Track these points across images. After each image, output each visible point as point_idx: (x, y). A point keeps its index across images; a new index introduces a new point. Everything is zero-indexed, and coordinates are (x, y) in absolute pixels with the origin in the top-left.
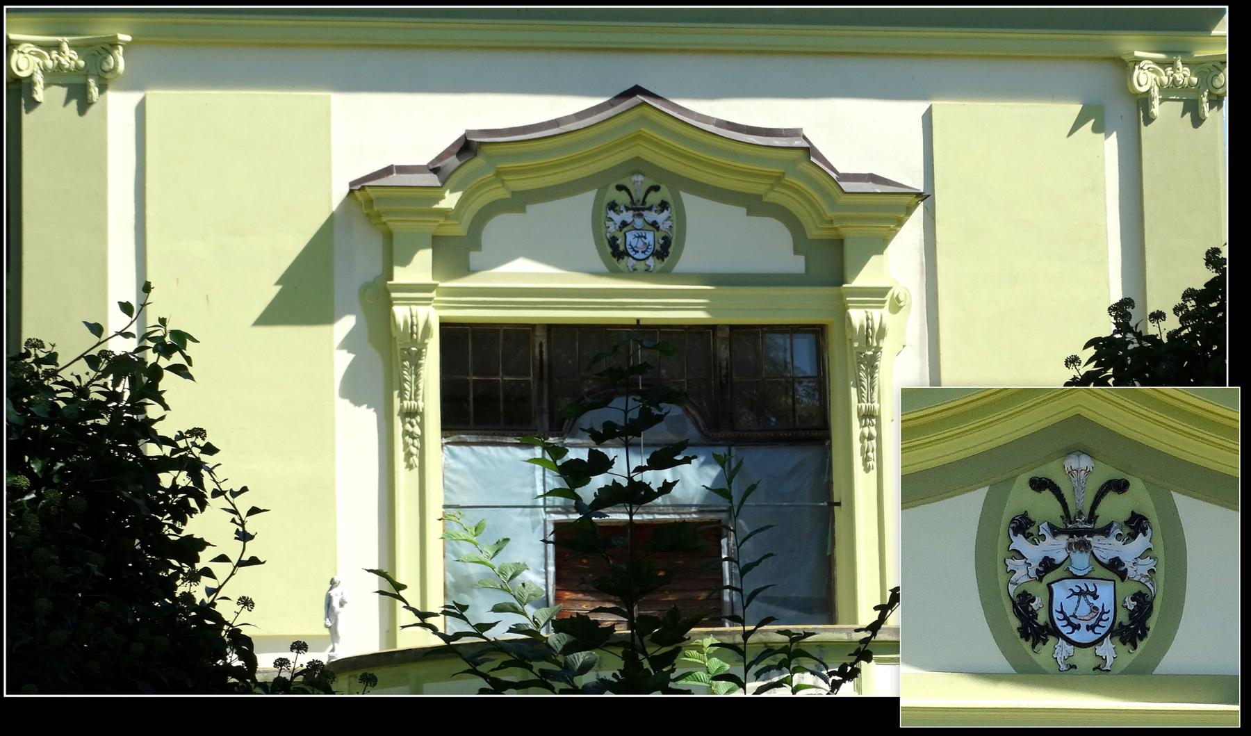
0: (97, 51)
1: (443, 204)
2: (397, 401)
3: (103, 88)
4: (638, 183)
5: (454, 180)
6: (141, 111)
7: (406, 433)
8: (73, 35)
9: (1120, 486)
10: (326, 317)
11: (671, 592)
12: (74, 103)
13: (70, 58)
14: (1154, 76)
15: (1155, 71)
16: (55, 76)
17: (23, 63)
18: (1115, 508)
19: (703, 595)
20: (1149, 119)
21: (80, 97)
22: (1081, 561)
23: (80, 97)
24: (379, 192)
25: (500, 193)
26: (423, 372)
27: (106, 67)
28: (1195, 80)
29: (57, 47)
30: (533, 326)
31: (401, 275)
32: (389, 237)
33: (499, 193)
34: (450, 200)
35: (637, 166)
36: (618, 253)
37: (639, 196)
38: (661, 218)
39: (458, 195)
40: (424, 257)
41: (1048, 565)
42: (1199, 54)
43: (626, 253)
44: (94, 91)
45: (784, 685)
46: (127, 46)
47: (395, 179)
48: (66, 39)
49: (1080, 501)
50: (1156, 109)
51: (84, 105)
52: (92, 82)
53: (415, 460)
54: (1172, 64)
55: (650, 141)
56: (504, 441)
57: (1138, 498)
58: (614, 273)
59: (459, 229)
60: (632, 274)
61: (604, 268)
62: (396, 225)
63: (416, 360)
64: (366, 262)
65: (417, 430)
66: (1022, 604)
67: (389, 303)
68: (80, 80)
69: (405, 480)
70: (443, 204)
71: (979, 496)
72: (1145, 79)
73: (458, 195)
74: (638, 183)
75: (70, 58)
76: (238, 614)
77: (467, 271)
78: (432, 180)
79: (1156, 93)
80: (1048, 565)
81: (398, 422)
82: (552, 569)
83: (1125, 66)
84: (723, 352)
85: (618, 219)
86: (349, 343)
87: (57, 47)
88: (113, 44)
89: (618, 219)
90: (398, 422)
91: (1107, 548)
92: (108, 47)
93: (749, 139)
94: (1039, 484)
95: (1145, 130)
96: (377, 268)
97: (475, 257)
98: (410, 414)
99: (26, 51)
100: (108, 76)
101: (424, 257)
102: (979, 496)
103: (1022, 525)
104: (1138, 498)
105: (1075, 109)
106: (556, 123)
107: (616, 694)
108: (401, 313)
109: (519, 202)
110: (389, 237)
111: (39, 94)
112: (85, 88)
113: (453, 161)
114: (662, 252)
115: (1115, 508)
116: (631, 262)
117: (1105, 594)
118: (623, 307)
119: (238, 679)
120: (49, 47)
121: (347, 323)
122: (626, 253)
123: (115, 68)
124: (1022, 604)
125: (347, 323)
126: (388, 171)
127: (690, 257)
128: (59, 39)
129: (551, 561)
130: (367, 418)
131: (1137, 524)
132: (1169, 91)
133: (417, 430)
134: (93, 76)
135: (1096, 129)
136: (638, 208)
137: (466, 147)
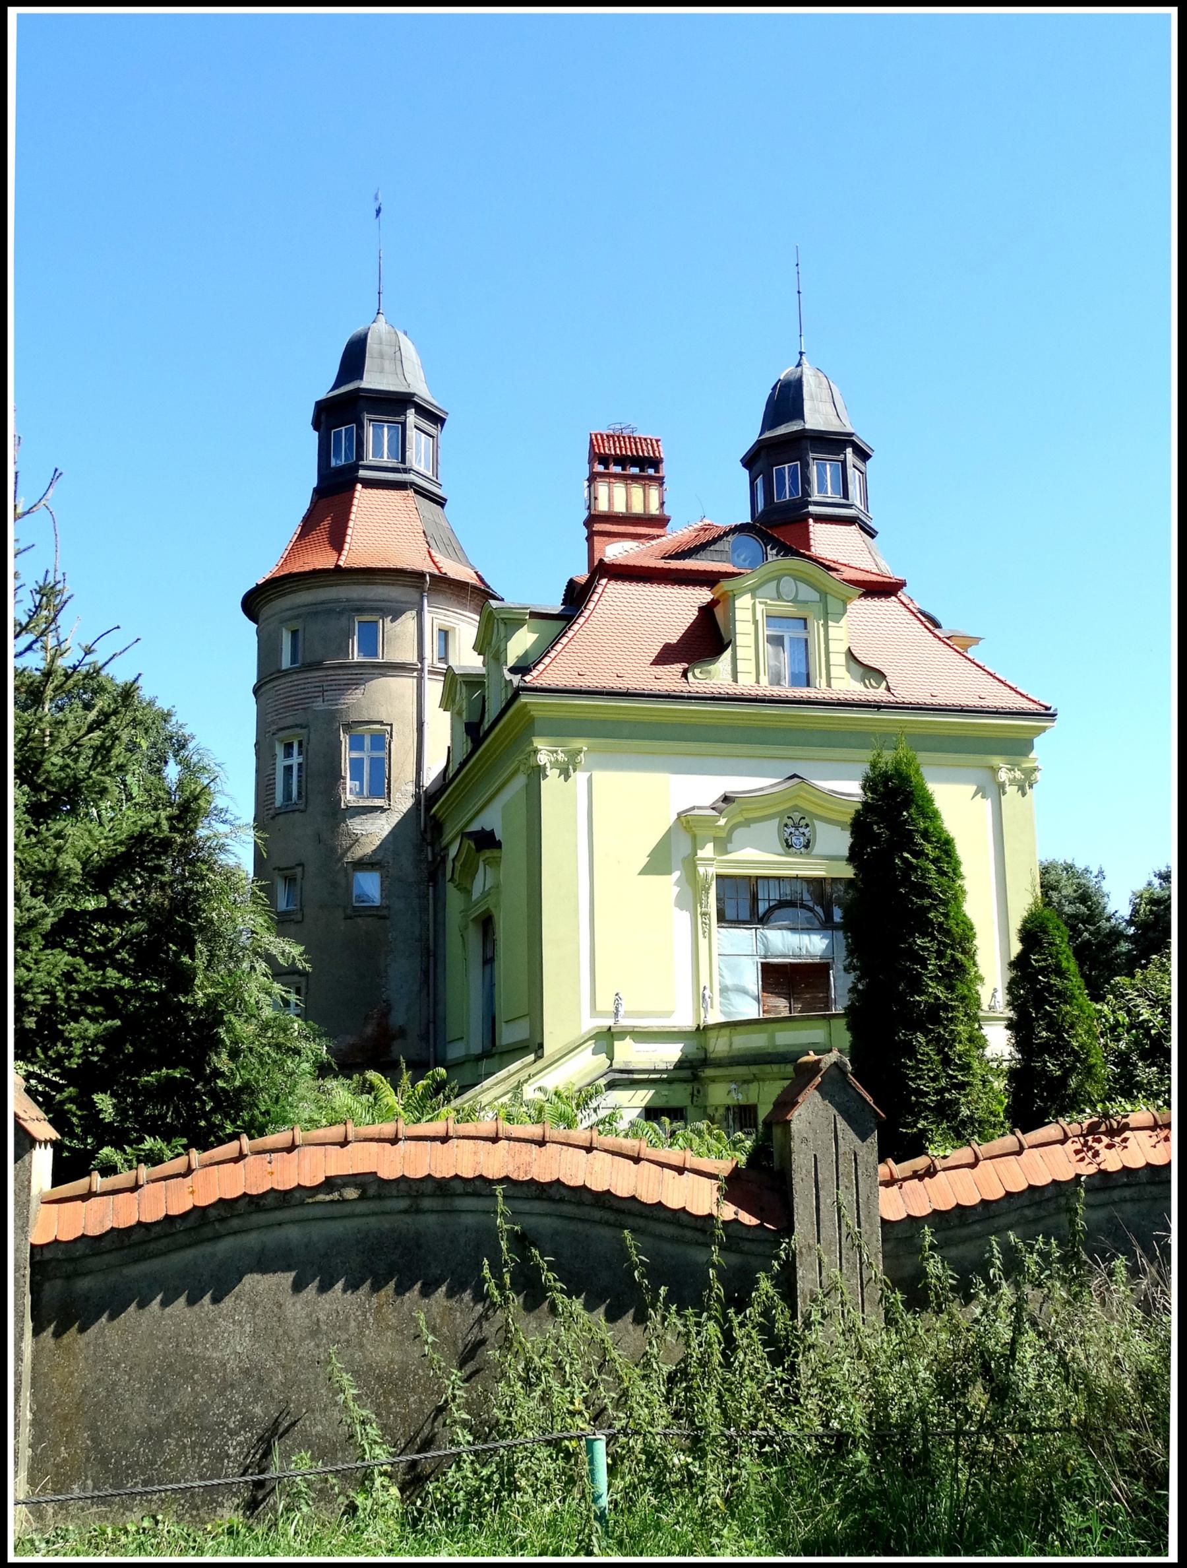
0: (573, 754)
1: (719, 823)
2: (699, 908)
3: (575, 770)
4: (797, 816)
5: (723, 813)
6: (590, 780)
7: (703, 922)
9: (804, 818)
10: (668, 872)
11: (808, 993)
12: (562, 776)
13: (561, 757)
16: (555, 764)
17: (543, 758)
18: (803, 822)
19: (821, 995)
20: (1004, 793)
21: (565, 773)
22: (797, 833)
23: (565, 773)
24: (693, 817)
25: (741, 819)
26: (710, 895)
29: (556, 752)
30: (750, 877)
31: (701, 854)
32: (694, 837)
33: (740, 819)
34: (722, 822)
35: (796, 808)
36: (789, 846)
37: (797, 821)
38: (806, 831)
39: (725, 820)
40: (710, 847)
41: (791, 833)
42: (1024, 766)
43: (792, 846)
44: (571, 771)
47: (696, 812)
49: (797, 821)
50: (1008, 789)
51: (567, 777)
52: (571, 767)
53: (707, 934)
54: (1013, 770)
55: (804, 798)
57: (807, 821)
58: (787, 854)
59: (724, 834)
60: (794, 855)
61: (783, 852)
62: (698, 832)
63: (707, 891)
64: (684, 847)
65: (707, 921)
66: (786, 841)
67: (695, 866)
68: (566, 766)
69: (703, 943)
70: (719, 823)
71: (778, 820)
72: (1003, 776)
73: (725, 820)
74: (797, 816)
75: (561, 757)
77: (728, 853)
78: (714, 813)
79: (1007, 782)
80: (791, 833)
81: (699, 917)
82: (760, 983)
83: (994, 770)
84: (828, 889)
85: (789, 831)
86: (677, 883)
87: (556, 752)
89: (789, 831)
90: (699, 917)
91: (802, 830)
94: (789, 818)
95: (1003, 798)
96: (689, 851)
97: (729, 846)
98: (704, 914)
101: (710, 847)
102: (778, 820)
103: (786, 825)
104: (807, 821)
105: (975, 788)
106: (762, 789)
108: (701, 870)
109: (748, 823)
110: (694, 837)
111: (548, 772)
112: (568, 769)
113: (720, 804)
114: (807, 846)
115: (803, 822)
116: (794, 850)
117: (802, 840)
118: (792, 869)
120: (553, 752)
121: (677, 874)
122: (792, 846)
124: (786, 841)
125: (677, 874)
126: (693, 808)
127: (819, 848)
129: (760, 979)
130: (686, 916)
131: (807, 826)
132: (1013, 782)
133: (707, 921)
135: (983, 797)
136: (797, 827)
137: (726, 799)
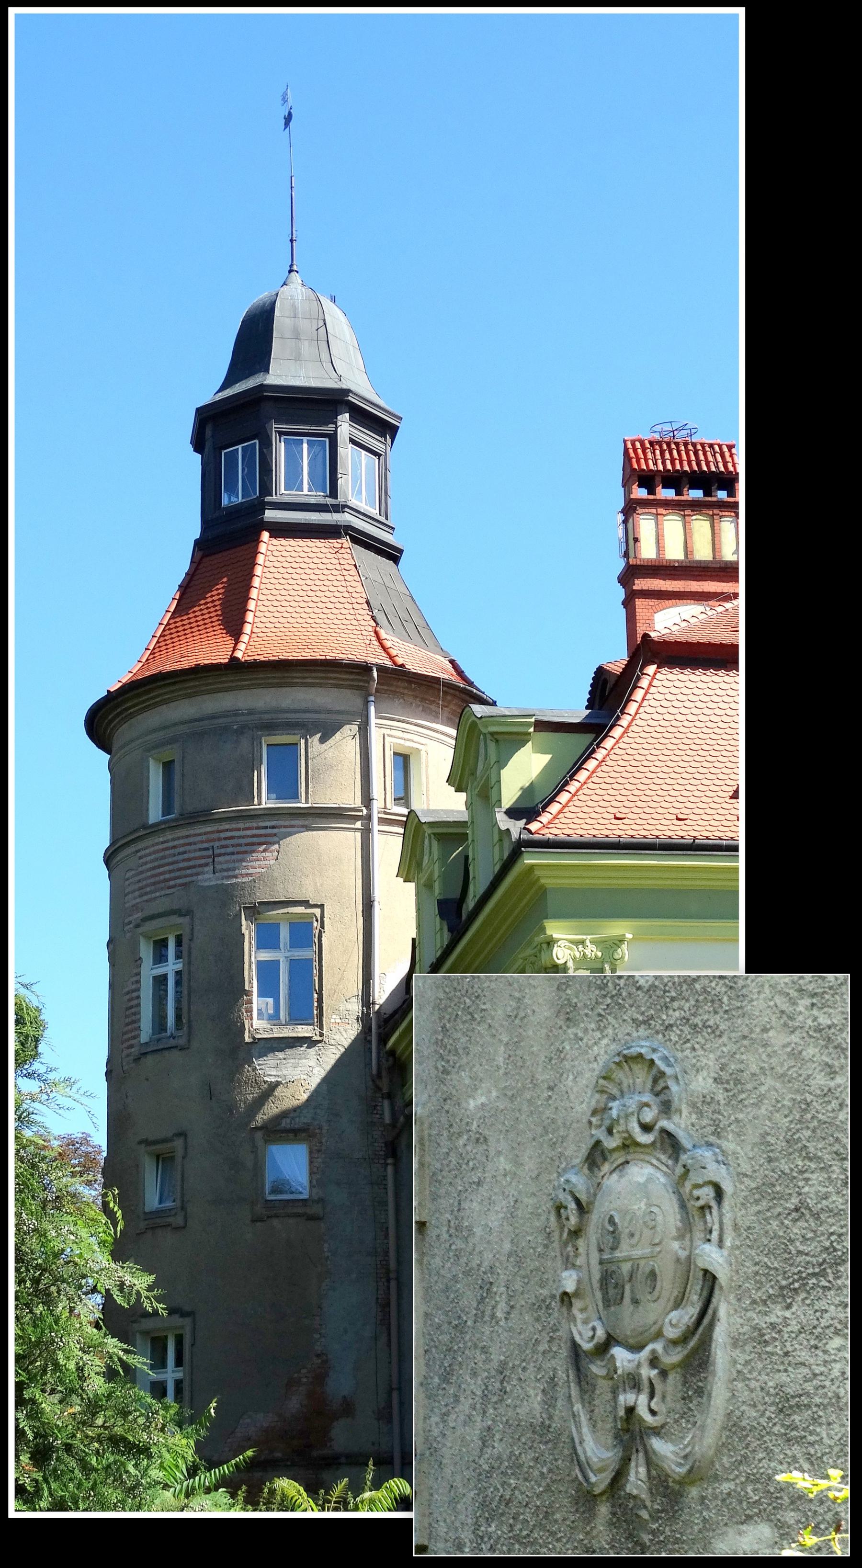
8: (592, 934)
14: (569, 952)
15: (570, 948)
27: (616, 957)
28: (599, 954)
29: (583, 942)
45: (388, 437)
46: (630, 942)
48: (589, 937)
56: (161, 733)
76: (290, 271)
88: (621, 940)
92: (618, 943)
93: (266, 955)
99: (562, 946)
100: (618, 962)
107: (366, 466)
119: (253, 764)
120: (577, 943)
123: (622, 958)
128: (584, 937)
134: (607, 962)
